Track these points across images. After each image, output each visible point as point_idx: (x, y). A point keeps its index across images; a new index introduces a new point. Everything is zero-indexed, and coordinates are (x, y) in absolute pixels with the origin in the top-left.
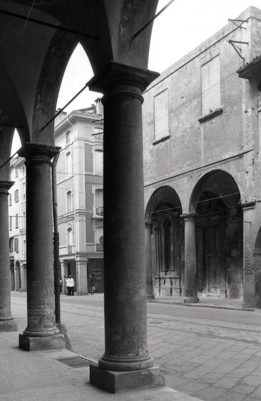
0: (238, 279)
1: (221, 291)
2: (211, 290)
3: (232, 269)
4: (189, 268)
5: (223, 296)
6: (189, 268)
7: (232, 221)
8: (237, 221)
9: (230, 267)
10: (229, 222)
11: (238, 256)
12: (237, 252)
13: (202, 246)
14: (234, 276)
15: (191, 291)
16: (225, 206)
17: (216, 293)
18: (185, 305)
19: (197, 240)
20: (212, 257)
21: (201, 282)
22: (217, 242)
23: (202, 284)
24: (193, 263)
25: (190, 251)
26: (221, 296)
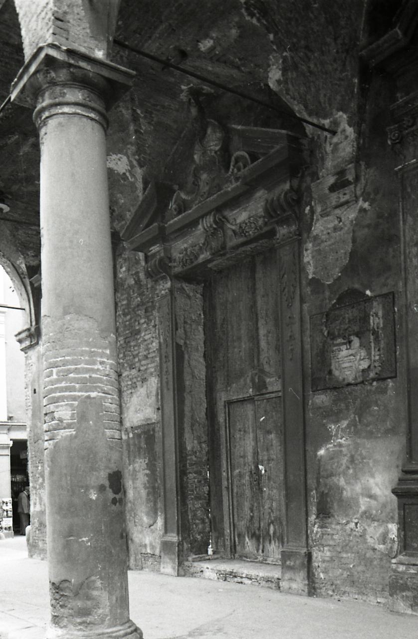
0: (371, 496)
1: (285, 556)
2: (244, 547)
3: (340, 445)
4: (64, 433)
5: (294, 586)
6: (64, 433)
7: (334, 198)
8: (359, 193)
9: (326, 438)
10: (319, 209)
11: (372, 375)
12: (363, 353)
13: (202, 360)
14: (348, 483)
15: (82, 590)
16: (297, 124)
17: (264, 562)
18: (199, 559)
19: (180, 331)
20: (243, 401)
21: (199, 513)
22: (262, 332)
23: (203, 522)
24: (93, 394)
25: (66, 312)
26: (284, 584)
